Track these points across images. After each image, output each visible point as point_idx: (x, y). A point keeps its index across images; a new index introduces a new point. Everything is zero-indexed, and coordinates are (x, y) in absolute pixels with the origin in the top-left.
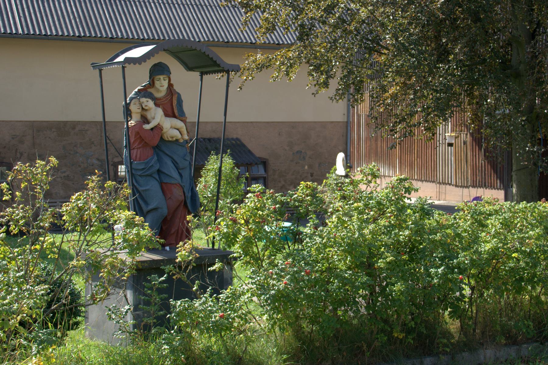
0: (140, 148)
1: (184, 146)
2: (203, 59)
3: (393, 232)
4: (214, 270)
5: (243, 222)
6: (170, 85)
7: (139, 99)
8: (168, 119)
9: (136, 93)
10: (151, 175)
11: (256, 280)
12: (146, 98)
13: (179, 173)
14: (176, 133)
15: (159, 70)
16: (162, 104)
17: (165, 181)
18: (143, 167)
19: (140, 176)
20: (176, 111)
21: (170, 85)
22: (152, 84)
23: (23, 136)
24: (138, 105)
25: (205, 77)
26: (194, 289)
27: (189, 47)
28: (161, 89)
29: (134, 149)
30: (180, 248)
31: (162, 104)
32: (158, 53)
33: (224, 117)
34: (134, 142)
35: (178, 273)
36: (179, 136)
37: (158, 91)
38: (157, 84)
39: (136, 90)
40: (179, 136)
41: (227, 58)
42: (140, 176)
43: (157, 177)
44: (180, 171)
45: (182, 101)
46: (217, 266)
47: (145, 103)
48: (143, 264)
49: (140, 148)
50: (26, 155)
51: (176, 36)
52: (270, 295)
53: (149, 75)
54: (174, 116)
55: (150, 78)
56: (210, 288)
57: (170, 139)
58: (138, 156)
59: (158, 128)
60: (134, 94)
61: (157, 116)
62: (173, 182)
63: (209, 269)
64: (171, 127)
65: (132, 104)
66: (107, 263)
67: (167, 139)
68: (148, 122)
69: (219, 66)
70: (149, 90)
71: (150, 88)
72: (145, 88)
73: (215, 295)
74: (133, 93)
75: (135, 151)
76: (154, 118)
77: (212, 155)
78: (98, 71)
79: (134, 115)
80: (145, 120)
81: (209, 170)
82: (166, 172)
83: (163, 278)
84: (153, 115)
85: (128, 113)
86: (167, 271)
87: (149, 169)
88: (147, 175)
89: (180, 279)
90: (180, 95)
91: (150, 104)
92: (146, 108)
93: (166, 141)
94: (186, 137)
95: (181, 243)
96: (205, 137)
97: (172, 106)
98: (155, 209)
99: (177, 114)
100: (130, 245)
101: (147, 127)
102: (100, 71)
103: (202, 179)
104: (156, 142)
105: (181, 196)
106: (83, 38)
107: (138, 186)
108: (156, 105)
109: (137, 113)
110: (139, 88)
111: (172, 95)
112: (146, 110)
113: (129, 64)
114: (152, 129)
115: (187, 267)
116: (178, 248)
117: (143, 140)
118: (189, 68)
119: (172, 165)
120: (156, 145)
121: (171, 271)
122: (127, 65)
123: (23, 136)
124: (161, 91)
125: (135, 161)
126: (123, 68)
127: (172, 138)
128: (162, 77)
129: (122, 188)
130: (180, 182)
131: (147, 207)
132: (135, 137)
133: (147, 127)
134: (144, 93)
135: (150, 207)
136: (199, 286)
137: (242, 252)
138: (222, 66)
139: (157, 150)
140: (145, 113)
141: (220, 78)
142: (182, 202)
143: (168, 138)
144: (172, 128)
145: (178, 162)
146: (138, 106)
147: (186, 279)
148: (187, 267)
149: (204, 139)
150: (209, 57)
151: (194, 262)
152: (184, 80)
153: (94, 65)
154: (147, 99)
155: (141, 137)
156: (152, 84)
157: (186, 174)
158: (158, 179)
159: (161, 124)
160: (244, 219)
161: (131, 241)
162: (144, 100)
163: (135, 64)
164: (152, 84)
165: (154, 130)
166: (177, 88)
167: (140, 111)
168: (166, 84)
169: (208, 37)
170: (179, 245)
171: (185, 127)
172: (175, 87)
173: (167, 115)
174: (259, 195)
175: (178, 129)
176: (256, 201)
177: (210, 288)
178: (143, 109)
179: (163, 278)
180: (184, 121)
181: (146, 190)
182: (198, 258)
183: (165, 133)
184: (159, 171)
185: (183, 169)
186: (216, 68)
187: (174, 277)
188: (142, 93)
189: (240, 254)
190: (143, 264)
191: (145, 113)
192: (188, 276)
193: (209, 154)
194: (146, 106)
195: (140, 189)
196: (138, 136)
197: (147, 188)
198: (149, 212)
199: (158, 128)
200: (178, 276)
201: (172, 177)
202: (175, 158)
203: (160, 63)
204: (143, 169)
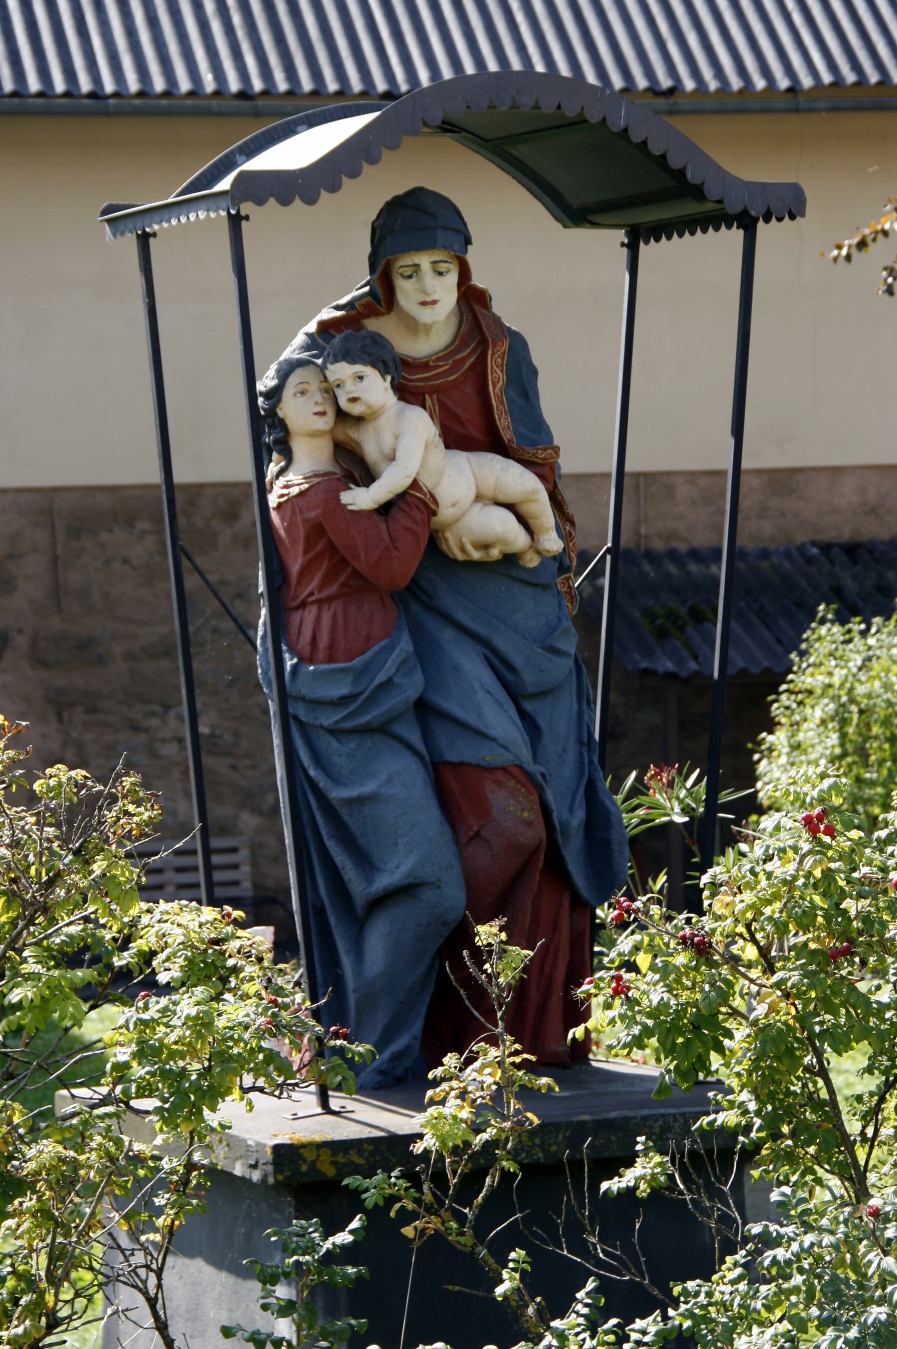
0: (329, 600)
1: (545, 587)
2: (626, 170)
3: (167, 1106)
4: (630, 1191)
5: (751, 953)
6: (472, 299)
7: (322, 369)
8: (462, 459)
9: (312, 343)
10: (382, 729)
11: (795, 1247)
12: (352, 361)
13: (523, 714)
14: (503, 527)
15: (415, 224)
16: (433, 391)
17: (452, 756)
18: (344, 690)
19: (333, 732)
20: (503, 421)
21: (472, 299)
22: (382, 296)
23: (11, 557)
24: (318, 397)
25: (648, 251)
26: (500, 1290)
27: (548, 106)
28: (425, 315)
29: (303, 605)
30: (445, 1086)
31: (433, 391)
32: (394, 146)
33: (732, 441)
34: (302, 574)
35: (430, 1210)
36: (518, 538)
37: (413, 326)
38: (407, 292)
39: (312, 327)
40: (518, 538)
41: (745, 162)
42: (333, 732)
43: (415, 737)
44: (528, 706)
45: (535, 372)
46: (642, 1172)
47: (350, 388)
48: (340, 1158)
49: (329, 600)
50: (22, 642)
51: (707, 73)
52: (863, 1327)
53: (368, 249)
54: (497, 446)
55: (372, 270)
56: (591, 1285)
57: (476, 555)
58: (324, 641)
59: (414, 502)
60: (306, 348)
61: (409, 446)
62: (489, 756)
63: (604, 1186)
64: (479, 498)
65: (288, 393)
66: (31, 1166)
67: (460, 556)
68: (366, 475)
69: (697, 193)
70: (373, 325)
71: (378, 314)
72: (354, 317)
73: (614, 1321)
74: (300, 339)
75: (310, 613)
76: (392, 458)
77: (823, 621)
78: (130, 242)
79: (298, 446)
80: (354, 467)
81: (810, 692)
82: (456, 711)
83: (343, 1238)
84: (387, 441)
85: (269, 434)
86: (371, 1198)
87: (372, 700)
88: (365, 730)
89: (439, 1238)
90: (524, 343)
91: (373, 389)
92: (356, 409)
93: (455, 561)
94: (553, 543)
95: (451, 1060)
96: (829, 535)
97: (482, 392)
98: (406, 890)
99: (507, 435)
100: (165, 1075)
101: (361, 499)
102: (144, 240)
103: (778, 739)
104: (405, 565)
105: (530, 824)
106: (260, 103)
107: (323, 782)
108: (406, 393)
109: (315, 434)
110: (328, 314)
111: (483, 343)
112: (359, 420)
113: (260, 202)
114: (385, 509)
115: (472, 1181)
116: (435, 1083)
117: (343, 562)
118: (575, 214)
119: (488, 677)
120: (406, 581)
121: (398, 1199)
122: (246, 208)
123: (11, 557)
124: (428, 329)
125: (311, 661)
126: (236, 221)
127: (485, 547)
128: (424, 260)
129: (114, 799)
130: (525, 753)
131: (369, 880)
132: (306, 551)
133: (361, 499)
134: (349, 336)
135: (384, 881)
136: (524, 1274)
137: (752, 1106)
138: (712, 191)
139: (415, 607)
140: (353, 433)
141: (848, 258)
142: (536, 850)
143: (463, 549)
144: (479, 500)
145: (518, 661)
146: (315, 400)
147: (467, 1240)
148: (472, 1181)
149: (826, 548)
150: (649, 154)
151: (514, 1155)
152: (535, 264)
153: (117, 219)
154: (359, 368)
155: (332, 547)
156: (382, 296)
157: (557, 718)
158: (420, 746)
159: (427, 482)
160: (755, 942)
161: (173, 1055)
162: (341, 371)
163: (285, 201)
164: (380, 293)
165: (394, 511)
166: (505, 308)
167: (326, 423)
168: (446, 291)
169: (832, 66)
170: (438, 1072)
171: (544, 496)
172: (497, 308)
173: (455, 438)
174: (820, 818)
175: (510, 507)
176: (806, 847)
177: (591, 1285)
178: (341, 415)
179: (343, 1238)
180: (545, 469)
181: (360, 800)
182: (534, 1132)
183: (448, 525)
184: (424, 709)
185: (541, 694)
186: (690, 208)
187: (408, 1231)
188: (338, 338)
189: (745, 1112)
190: (340, 1158)
191: (353, 433)
192: (481, 1229)
193: (806, 617)
194: (354, 400)
195: (336, 794)
196: (319, 547)
197: (369, 788)
198: (378, 903)
199: (414, 502)
200: (432, 1224)
201: (485, 736)
202: (504, 643)
203: (421, 190)
204: (345, 700)
